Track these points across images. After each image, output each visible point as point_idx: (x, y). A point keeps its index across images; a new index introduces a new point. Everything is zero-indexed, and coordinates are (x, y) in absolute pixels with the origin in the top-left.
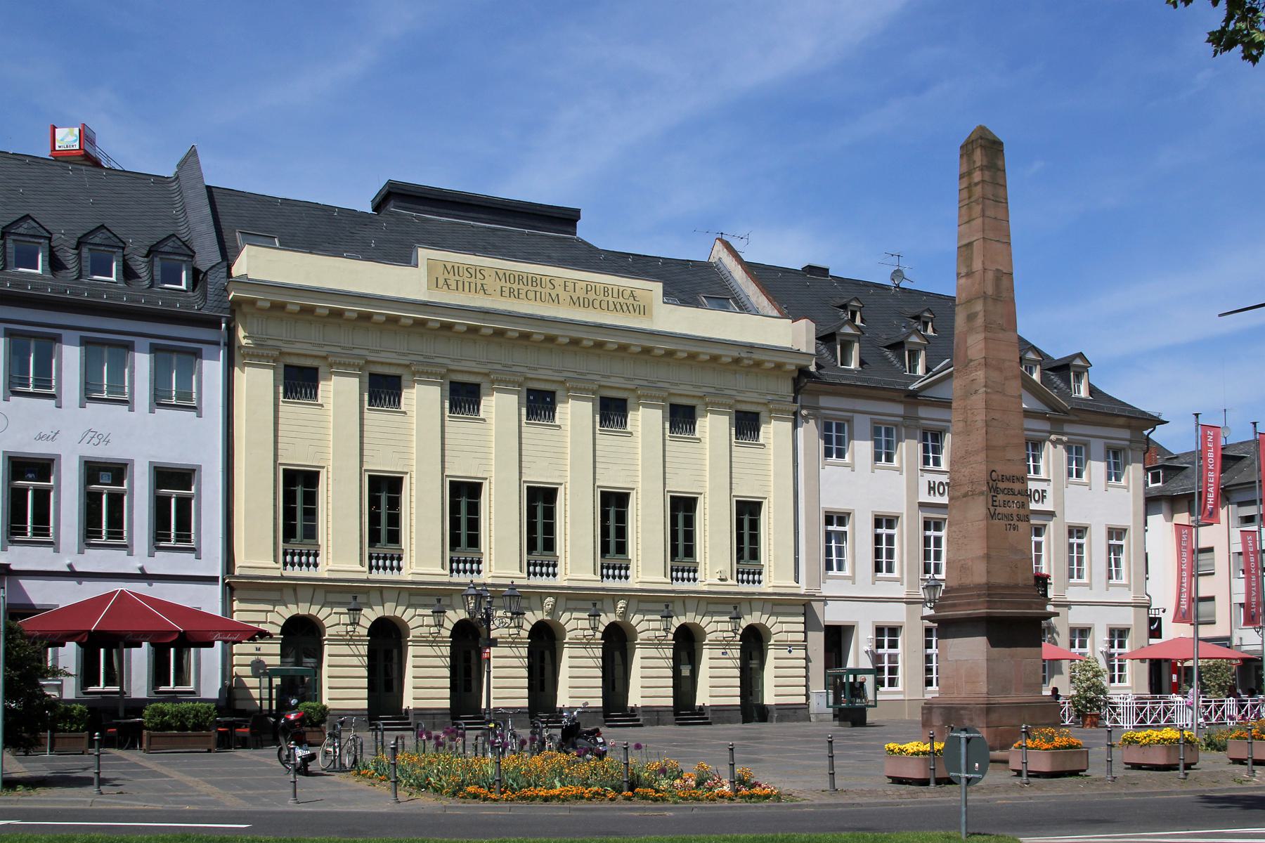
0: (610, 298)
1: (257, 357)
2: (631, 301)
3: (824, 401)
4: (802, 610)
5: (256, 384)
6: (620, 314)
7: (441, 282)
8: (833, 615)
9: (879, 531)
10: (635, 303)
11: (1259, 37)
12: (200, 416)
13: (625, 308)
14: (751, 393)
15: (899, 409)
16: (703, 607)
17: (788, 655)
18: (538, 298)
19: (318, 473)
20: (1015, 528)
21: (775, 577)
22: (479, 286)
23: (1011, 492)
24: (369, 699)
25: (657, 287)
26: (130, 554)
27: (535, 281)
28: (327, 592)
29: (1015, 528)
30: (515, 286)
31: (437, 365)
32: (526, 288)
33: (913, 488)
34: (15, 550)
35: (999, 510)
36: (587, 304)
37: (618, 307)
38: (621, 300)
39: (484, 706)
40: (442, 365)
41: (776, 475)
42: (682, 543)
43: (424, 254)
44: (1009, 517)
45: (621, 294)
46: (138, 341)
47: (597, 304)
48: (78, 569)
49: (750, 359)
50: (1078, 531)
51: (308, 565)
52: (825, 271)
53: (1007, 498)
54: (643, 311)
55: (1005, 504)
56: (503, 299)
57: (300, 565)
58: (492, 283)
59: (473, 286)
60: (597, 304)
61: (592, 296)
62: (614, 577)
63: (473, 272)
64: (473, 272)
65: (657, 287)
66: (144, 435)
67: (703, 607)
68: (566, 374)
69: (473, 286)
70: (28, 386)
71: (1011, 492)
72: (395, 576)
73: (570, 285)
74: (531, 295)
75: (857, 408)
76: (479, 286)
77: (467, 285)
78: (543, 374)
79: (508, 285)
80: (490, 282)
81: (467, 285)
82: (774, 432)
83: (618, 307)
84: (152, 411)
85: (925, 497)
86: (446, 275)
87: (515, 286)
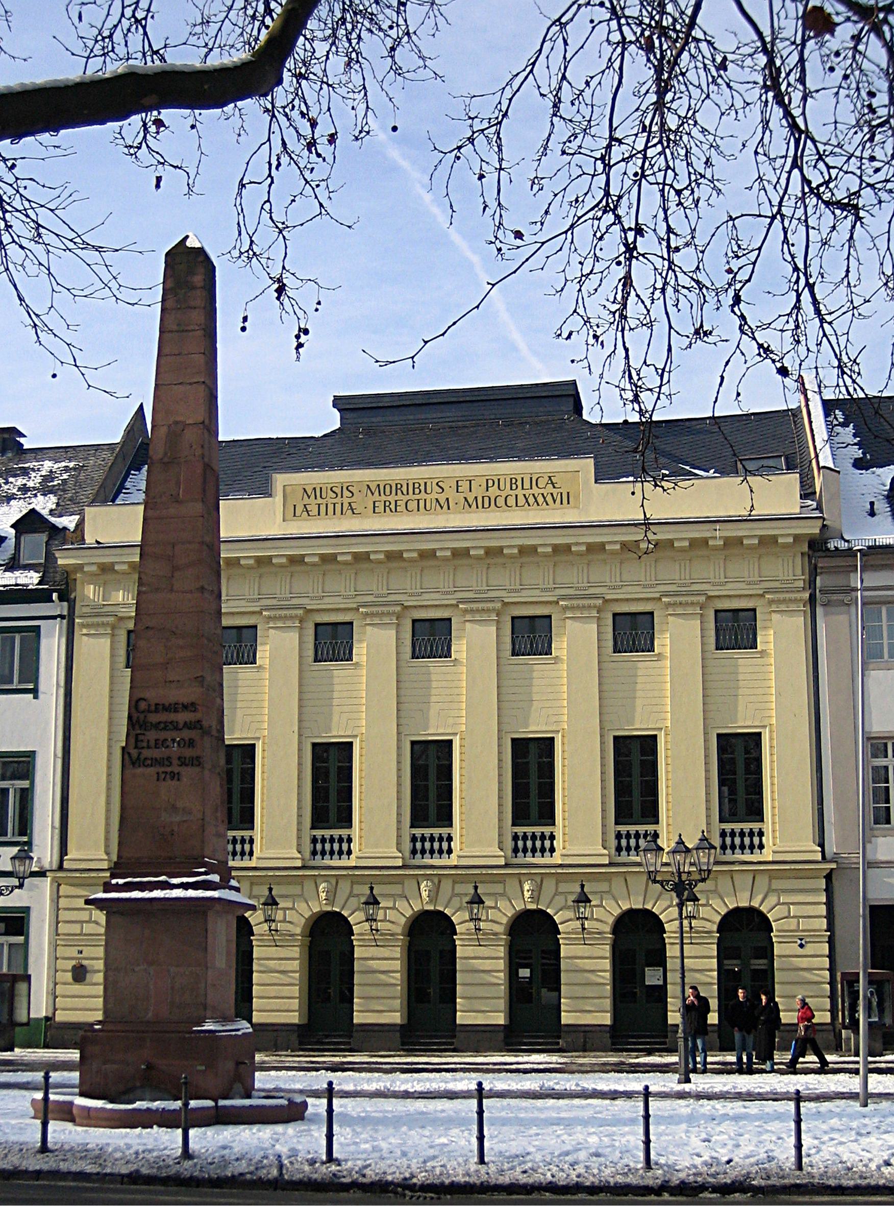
0: (520, 492)
4: (823, 883)
10: (555, 491)
12: (36, 697)
13: (540, 499)
14: (735, 584)
18: (423, 507)
22: (346, 506)
25: (587, 465)
27: (417, 487)
30: (392, 498)
31: (491, 600)
32: (406, 498)
37: (531, 500)
38: (535, 490)
40: (699, 593)
41: (778, 694)
43: (280, 480)
45: (534, 482)
47: (501, 501)
49: (577, 544)
50: (192, 797)
54: (566, 499)
58: (363, 501)
59: (338, 507)
60: (501, 501)
61: (493, 491)
63: (338, 491)
64: (338, 491)
65: (587, 465)
68: (359, 599)
69: (338, 507)
70: (11, 682)
73: (464, 486)
74: (412, 505)
76: (346, 506)
77: (331, 507)
78: (429, 599)
79: (383, 498)
81: (331, 507)
82: (781, 635)
83: (531, 500)
86: (306, 500)
87: (392, 498)
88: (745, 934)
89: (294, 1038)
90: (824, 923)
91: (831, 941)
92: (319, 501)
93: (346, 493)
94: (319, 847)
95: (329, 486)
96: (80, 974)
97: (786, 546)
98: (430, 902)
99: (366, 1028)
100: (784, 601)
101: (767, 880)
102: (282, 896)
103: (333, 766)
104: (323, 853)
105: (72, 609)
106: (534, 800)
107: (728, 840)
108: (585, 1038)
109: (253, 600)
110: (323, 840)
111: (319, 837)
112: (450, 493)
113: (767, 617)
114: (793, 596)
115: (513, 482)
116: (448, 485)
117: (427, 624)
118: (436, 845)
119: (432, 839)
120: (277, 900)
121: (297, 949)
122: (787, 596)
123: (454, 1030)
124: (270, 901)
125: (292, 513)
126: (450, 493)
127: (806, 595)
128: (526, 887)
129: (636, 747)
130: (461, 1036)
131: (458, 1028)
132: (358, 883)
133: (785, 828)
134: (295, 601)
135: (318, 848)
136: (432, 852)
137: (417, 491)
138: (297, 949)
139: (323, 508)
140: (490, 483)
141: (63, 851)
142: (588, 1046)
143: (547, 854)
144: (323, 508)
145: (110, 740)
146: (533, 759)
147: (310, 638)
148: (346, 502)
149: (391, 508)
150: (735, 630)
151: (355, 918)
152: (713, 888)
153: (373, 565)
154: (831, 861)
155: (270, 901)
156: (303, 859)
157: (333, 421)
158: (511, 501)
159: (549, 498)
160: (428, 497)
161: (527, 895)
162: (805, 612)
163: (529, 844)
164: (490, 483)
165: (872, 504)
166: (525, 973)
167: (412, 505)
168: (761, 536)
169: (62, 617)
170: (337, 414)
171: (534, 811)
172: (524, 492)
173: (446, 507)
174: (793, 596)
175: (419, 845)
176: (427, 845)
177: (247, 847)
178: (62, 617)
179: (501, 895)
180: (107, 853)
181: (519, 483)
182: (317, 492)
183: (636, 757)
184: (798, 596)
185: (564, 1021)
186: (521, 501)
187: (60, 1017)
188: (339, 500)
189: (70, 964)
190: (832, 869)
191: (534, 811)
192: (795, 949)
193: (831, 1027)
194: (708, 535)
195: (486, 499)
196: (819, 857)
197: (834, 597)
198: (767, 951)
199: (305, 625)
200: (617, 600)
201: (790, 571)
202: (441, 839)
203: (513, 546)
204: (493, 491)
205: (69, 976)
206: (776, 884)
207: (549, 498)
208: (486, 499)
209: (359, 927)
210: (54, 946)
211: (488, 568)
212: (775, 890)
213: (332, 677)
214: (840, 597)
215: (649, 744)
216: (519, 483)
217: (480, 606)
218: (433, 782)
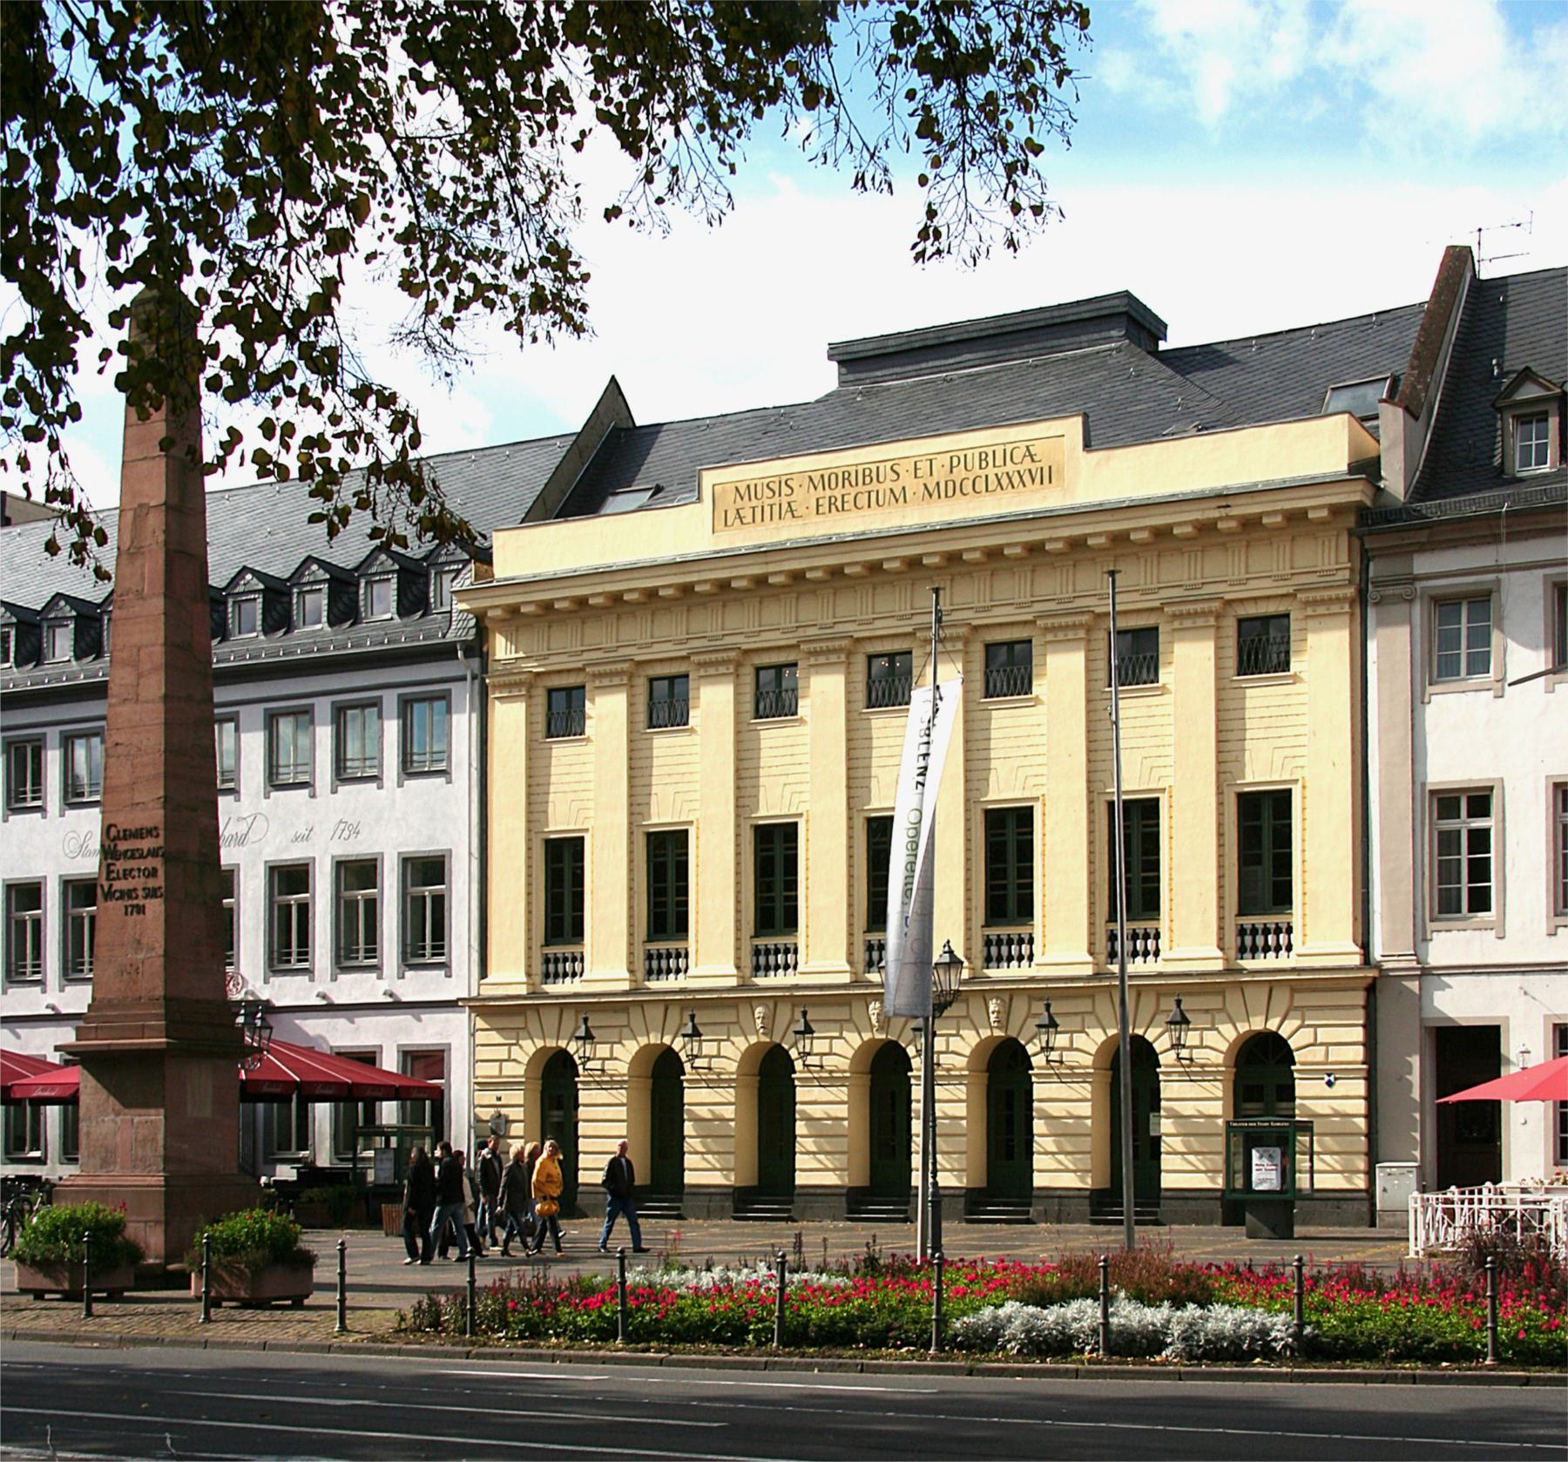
0: (991, 471)
2: (1028, 464)
3: (1423, 564)
4: (1359, 998)
7: (731, 515)
8: (1459, 1003)
9: (1449, 825)
10: (1034, 467)
11: (421, 4)
13: (1016, 479)
14: (1256, 578)
16: (1281, 999)
17: (1328, 1091)
19: (582, 839)
20: (141, 910)
21: (1320, 931)
22: (785, 506)
26: (312, 980)
27: (869, 475)
28: (1293, 991)
29: (141, 910)
30: (838, 493)
32: (853, 491)
34: (17, 992)
35: (118, 885)
36: (954, 489)
37: (1005, 481)
38: (1010, 467)
39: (916, 1179)
43: (709, 478)
44: (129, 894)
45: (1009, 457)
46: (454, 687)
47: (968, 487)
48: (406, 998)
49: (1228, 518)
54: (1046, 476)
55: (127, 874)
56: (821, 518)
59: (776, 508)
60: (968, 487)
61: (960, 472)
63: (775, 487)
65: (1073, 427)
66: (394, 818)
67: (1281, 999)
68: (1038, 607)
69: (776, 508)
72: (1284, 961)
73: (924, 467)
77: (767, 509)
79: (828, 492)
80: (804, 498)
81: (767, 509)
82: (1322, 652)
83: (1005, 481)
87: (838, 493)
89: (729, 1204)
91: (1371, 1079)
92: (754, 502)
93: (785, 490)
94: (762, 960)
95: (784, 479)
97: (1322, 522)
98: (880, 1029)
99: (1049, 1193)
100: (1322, 602)
101: (1154, 1000)
107: (994, 950)
108: (1060, 1204)
109: (576, 654)
110: (1254, 932)
111: (994, 938)
113: (1302, 625)
114: (1333, 593)
116: (905, 468)
117: (1258, 623)
118: (1260, 940)
120: (701, 1029)
122: (1326, 594)
123: (681, 1193)
124: (1178, 1018)
125: (721, 520)
126: (907, 479)
127: (1350, 591)
128: (992, 1007)
129: (1011, 823)
130: (1165, 1206)
131: (581, 1189)
132: (1301, 991)
134: (728, 640)
137: (868, 480)
139: (758, 511)
140: (955, 461)
141: (484, 974)
142: (1064, 1215)
144: (758, 511)
145: (967, 801)
146: (1267, 823)
147: (749, 689)
148: (785, 500)
150: (1261, 648)
152: (1220, 1006)
153: (851, 583)
155: (1178, 1018)
156: (1226, 960)
157: (826, 378)
158: (980, 485)
159: (1026, 478)
160: (881, 487)
161: (993, 1017)
162: (1352, 615)
164: (955, 461)
168: (1243, 516)
172: (996, 470)
173: (901, 499)
174: (1333, 593)
179: (1219, 1010)
180: (850, 962)
181: (990, 459)
182: (751, 491)
184: (1341, 592)
186: (993, 483)
188: (776, 499)
190: (1375, 979)
193: (1364, 1195)
194: (1216, 514)
195: (950, 485)
197: (1389, 591)
199: (534, 692)
201: (1329, 559)
203: (1016, 544)
204: (960, 472)
206: (1300, 1000)
207: (1026, 478)
208: (950, 485)
209: (1167, 1058)
211: (1033, 571)
212: (1297, 1008)
213: (1244, 698)
214: (1398, 590)
215: (1024, 817)
217: (1191, 608)
218: (1012, 864)
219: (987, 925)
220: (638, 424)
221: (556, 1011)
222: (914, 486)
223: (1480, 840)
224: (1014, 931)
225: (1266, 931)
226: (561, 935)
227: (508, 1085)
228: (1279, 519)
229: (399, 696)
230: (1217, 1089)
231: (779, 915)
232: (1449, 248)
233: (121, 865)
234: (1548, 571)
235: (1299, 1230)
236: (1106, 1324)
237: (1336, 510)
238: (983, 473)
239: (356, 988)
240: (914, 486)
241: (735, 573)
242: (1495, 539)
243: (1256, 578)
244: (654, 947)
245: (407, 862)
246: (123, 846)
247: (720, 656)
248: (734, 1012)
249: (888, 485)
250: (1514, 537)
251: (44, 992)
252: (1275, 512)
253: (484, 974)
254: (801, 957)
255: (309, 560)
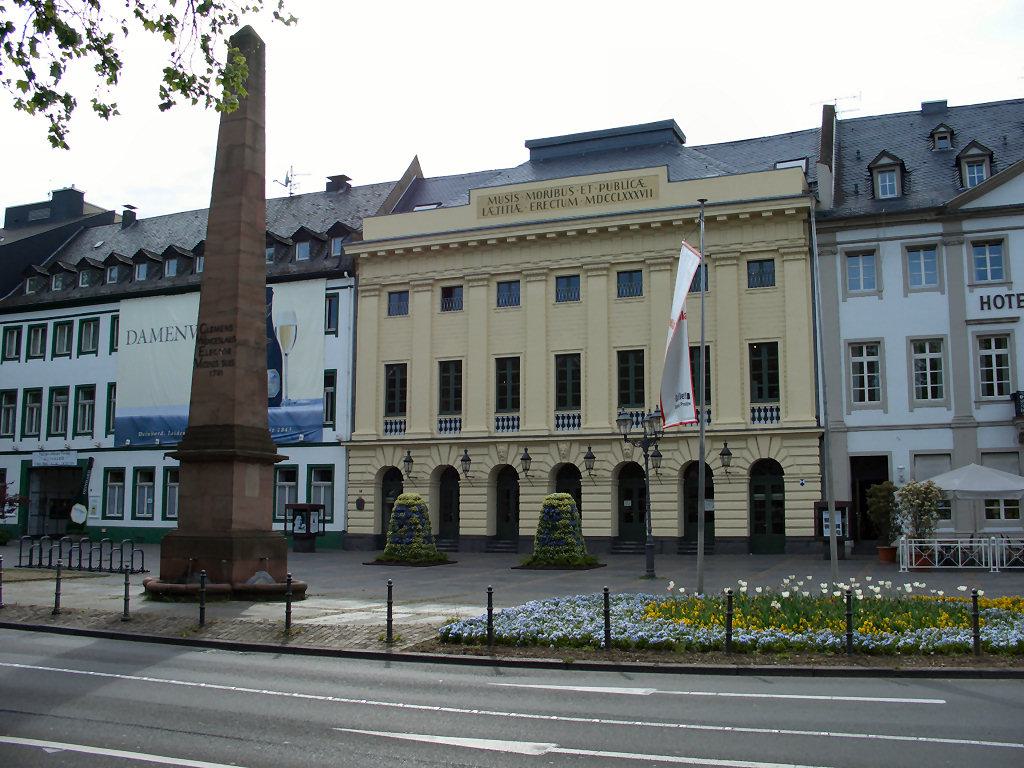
1: (377, 289)
3: (841, 237)
4: (816, 442)
5: (373, 306)
6: (597, 206)
12: (337, 336)
13: (634, 195)
15: (938, 228)
17: (802, 488)
20: (220, 373)
23: (220, 341)
24: (518, 528)
27: (557, 192)
30: (542, 200)
33: (957, 305)
37: (628, 196)
38: (630, 190)
42: (508, 394)
45: (630, 184)
51: (772, 419)
52: (661, 139)
53: (214, 347)
54: (650, 194)
55: (211, 352)
57: (766, 419)
62: (451, 429)
68: (466, 271)
71: (220, 341)
73: (586, 189)
74: (554, 204)
75: (882, 236)
77: (505, 208)
80: (525, 203)
81: (505, 208)
82: (792, 274)
83: (628, 196)
84: (906, 296)
85: (974, 312)
87: (542, 200)
88: (767, 477)
90: (817, 469)
91: (823, 481)
96: (360, 505)
102: (664, 451)
103: (569, 368)
104: (563, 426)
105: (357, 281)
106: (569, 395)
110: (503, 420)
112: (577, 194)
115: (616, 186)
117: (627, 275)
119: (569, 418)
121: (485, 489)
126: (577, 194)
129: (509, 364)
133: (797, 405)
135: (389, 428)
136: (569, 426)
138: (610, 488)
139: (500, 209)
141: (353, 430)
143: (775, 421)
144: (500, 209)
146: (632, 364)
149: (541, 207)
151: (582, 468)
154: (823, 427)
157: (525, 156)
159: (639, 194)
163: (393, 427)
165: (856, 186)
166: (628, 503)
167: (554, 204)
169: (351, 287)
170: (528, 151)
171: (632, 398)
175: (757, 414)
176: (506, 423)
177: (516, 423)
178: (351, 287)
179: (428, 456)
181: (620, 185)
183: (764, 357)
185: (460, 533)
186: (622, 196)
187: (351, 530)
189: (355, 498)
191: (632, 398)
192: (797, 486)
196: (815, 424)
198: (781, 489)
200: (618, 263)
202: (574, 417)
205: (354, 506)
207: (639, 194)
210: (347, 487)
214: (829, 248)
216: (620, 185)
219: (497, 412)
220: (426, 175)
221: (568, 444)
222: (581, 198)
223: (935, 364)
224: (398, 419)
225: (508, 420)
226: (448, 410)
227: (367, 483)
228: (725, 218)
229: (902, 244)
230: (675, 488)
231: (397, 405)
232: (672, 121)
233: (208, 347)
234: (902, 241)
235: (317, 550)
236: (58, 581)
237: (799, 210)
238: (617, 192)
239: (57, 443)
240: (581, 198)
241: (675, 218)
242: (878, 225)
243: (758, 241)
244: (388, 419)
245: (53, 390)
246: (210, 336)
247: (372, 287)
248: (745, 442)
249: (568, 197)
250: (888, 225)
251: (334, 430)
252: (791, 209)
253: (353, 430)
254: (781, 414)
255: (884, 154)
